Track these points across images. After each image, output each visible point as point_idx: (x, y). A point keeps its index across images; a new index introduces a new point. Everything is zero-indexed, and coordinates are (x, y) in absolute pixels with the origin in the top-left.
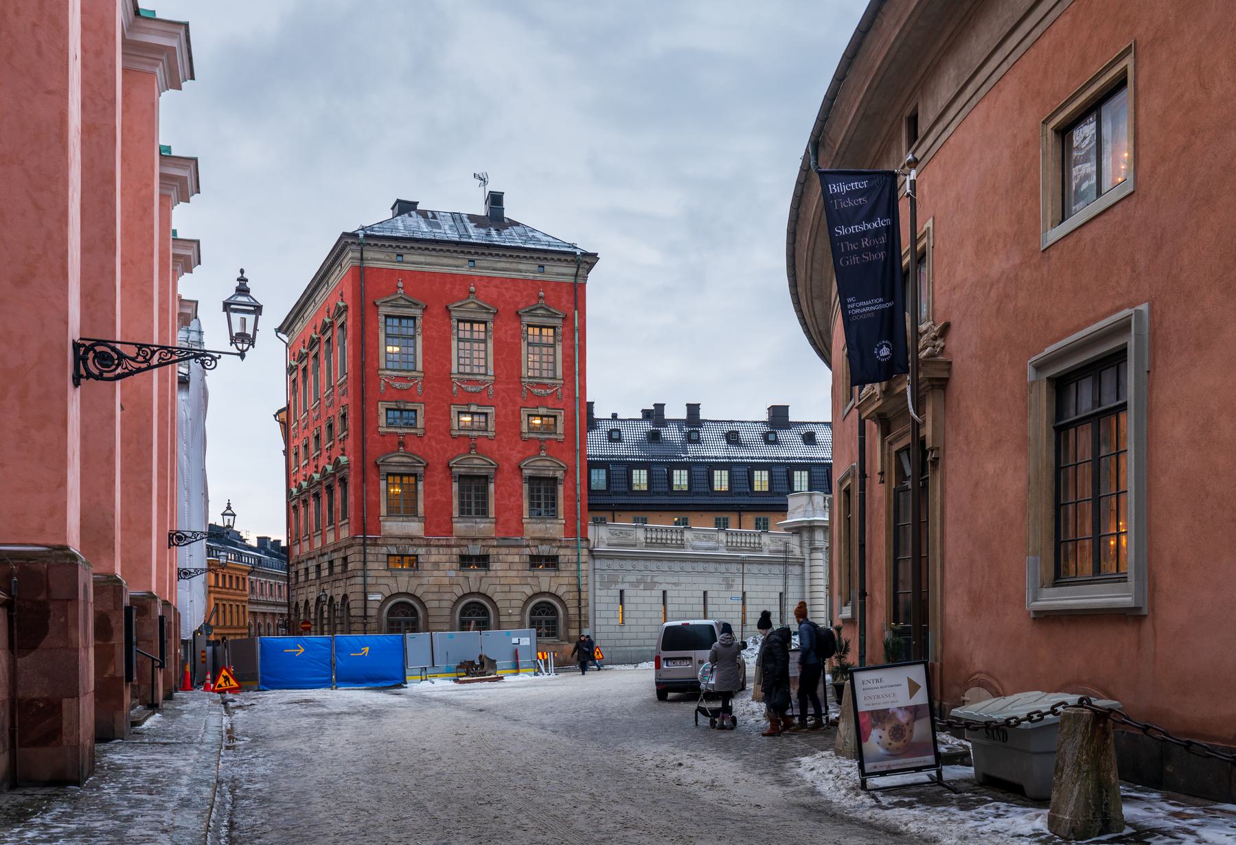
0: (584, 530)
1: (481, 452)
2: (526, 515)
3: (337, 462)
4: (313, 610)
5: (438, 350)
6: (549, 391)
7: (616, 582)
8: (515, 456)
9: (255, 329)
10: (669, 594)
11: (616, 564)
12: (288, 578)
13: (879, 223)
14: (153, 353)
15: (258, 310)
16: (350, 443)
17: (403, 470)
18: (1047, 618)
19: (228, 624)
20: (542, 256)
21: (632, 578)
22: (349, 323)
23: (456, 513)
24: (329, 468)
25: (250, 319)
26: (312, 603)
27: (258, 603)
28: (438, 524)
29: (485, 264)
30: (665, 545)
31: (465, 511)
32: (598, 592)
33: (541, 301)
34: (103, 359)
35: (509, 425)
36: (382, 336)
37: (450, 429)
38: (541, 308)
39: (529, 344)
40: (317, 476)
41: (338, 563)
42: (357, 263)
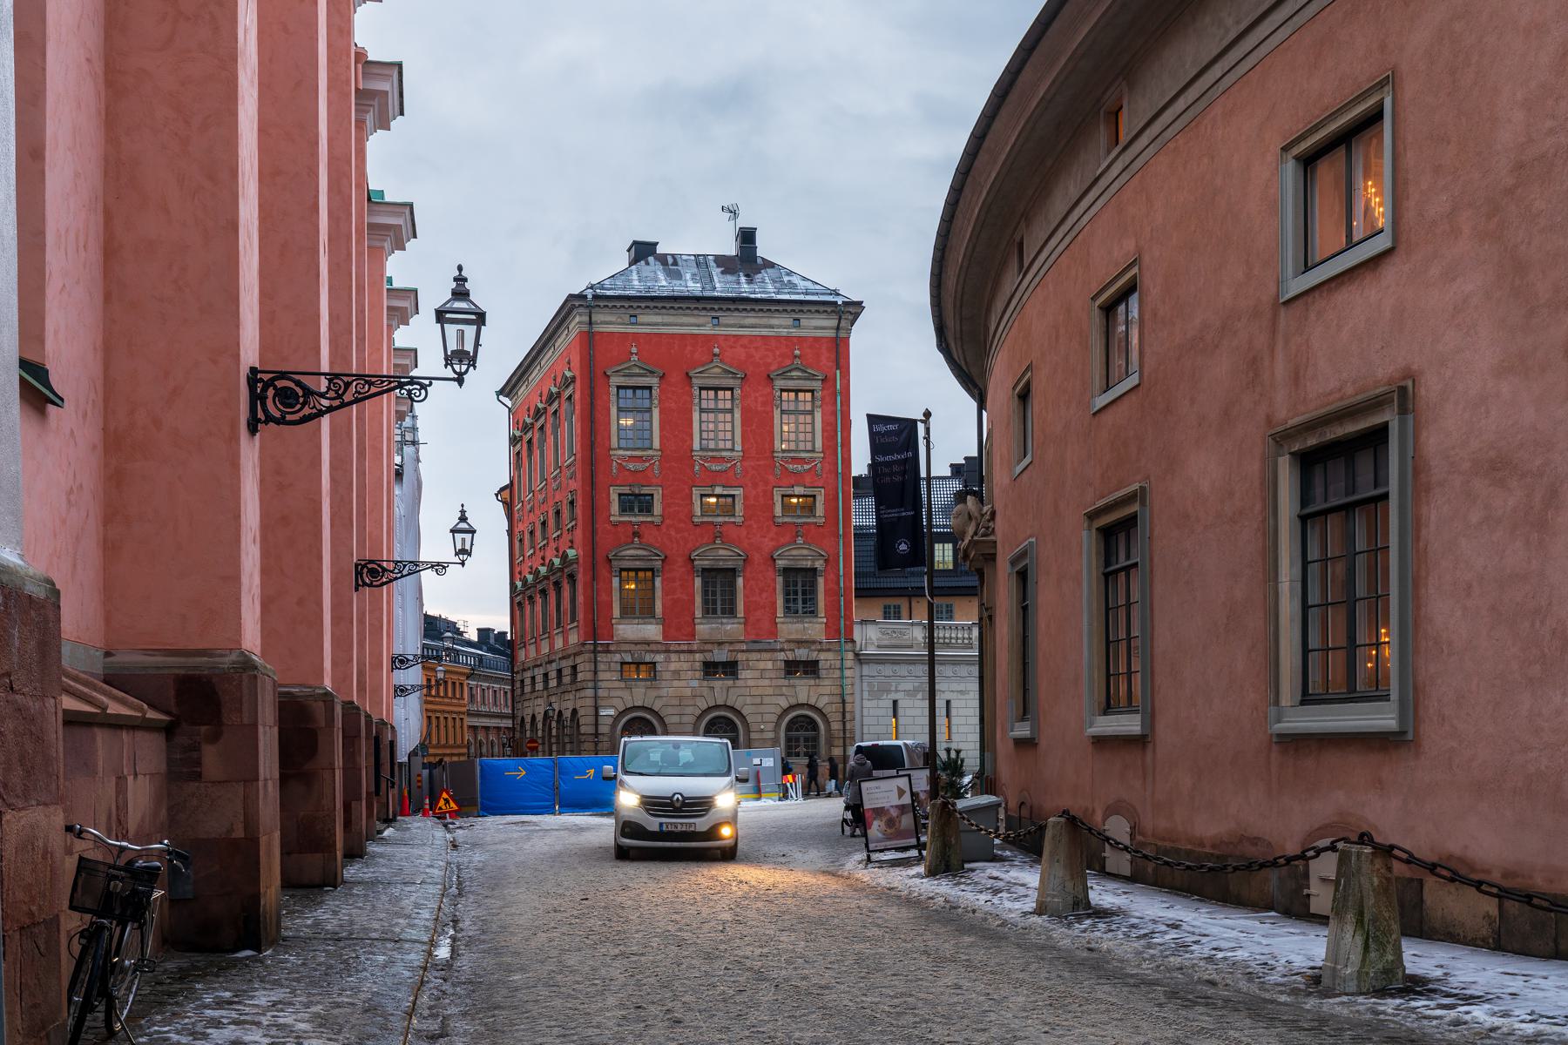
0: (849, 630)
1: (727, 541)
2: (780, 613)
3: (564, 557)
4: (540, 726)
5: (677, 425)
6: (807, 467)
7: (888, 691)
8: (768, 544)
9: (477, 344)
10: (953, 704)
11: (887, 670)
12: (513, 682)
13: (910, 454)
14: (347, 385)
15: (480, 319)
16: (579, 533)
17: (638, 564)
18: (1100, 742)
19: (443, 742)
20: (797, 308)
22: (577, 396)
23: (698, 613)
24: (557, 561)
25: (470, 331)
26: (540, 718)
27: (478, 715)
28: (678, 626)
29: (731, 321)
31: (709, 610)
32: (866, 704)
33: (797, 361)
34: (373, 573)
35: (759, 509)
36: (614, 410)
37: (691, 515)
38: (797, 369)
39: (783, 412)
40: (543, 570)
41: (567, 672)
42: (585, 328)
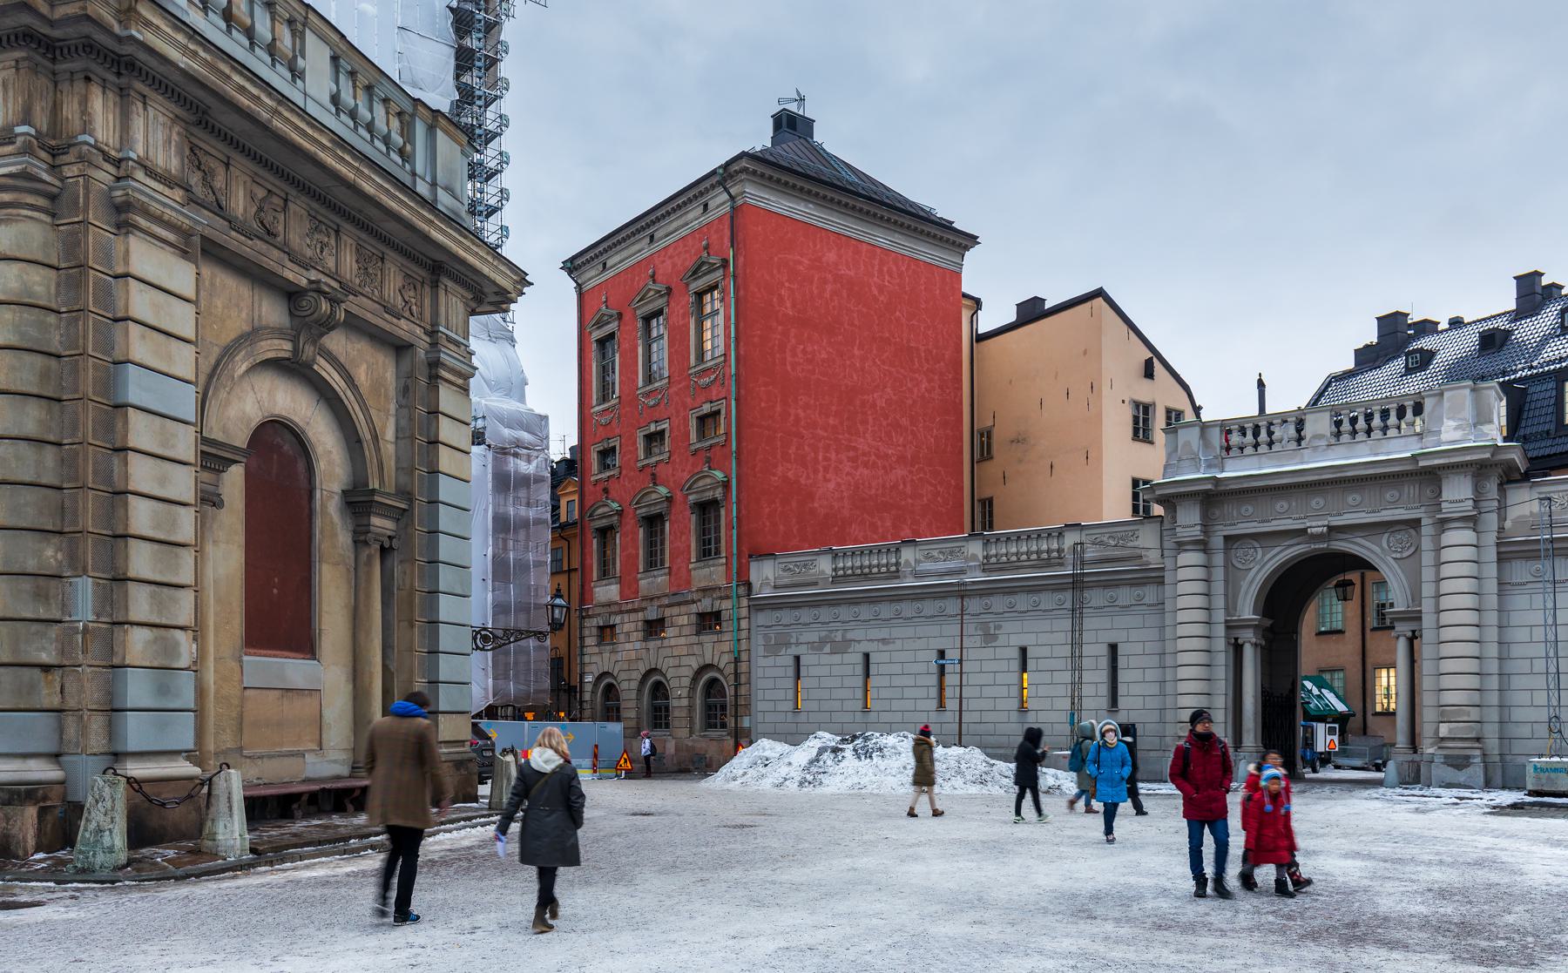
11: (787, 616)
21: (813, 636)
30: (866, 577)
